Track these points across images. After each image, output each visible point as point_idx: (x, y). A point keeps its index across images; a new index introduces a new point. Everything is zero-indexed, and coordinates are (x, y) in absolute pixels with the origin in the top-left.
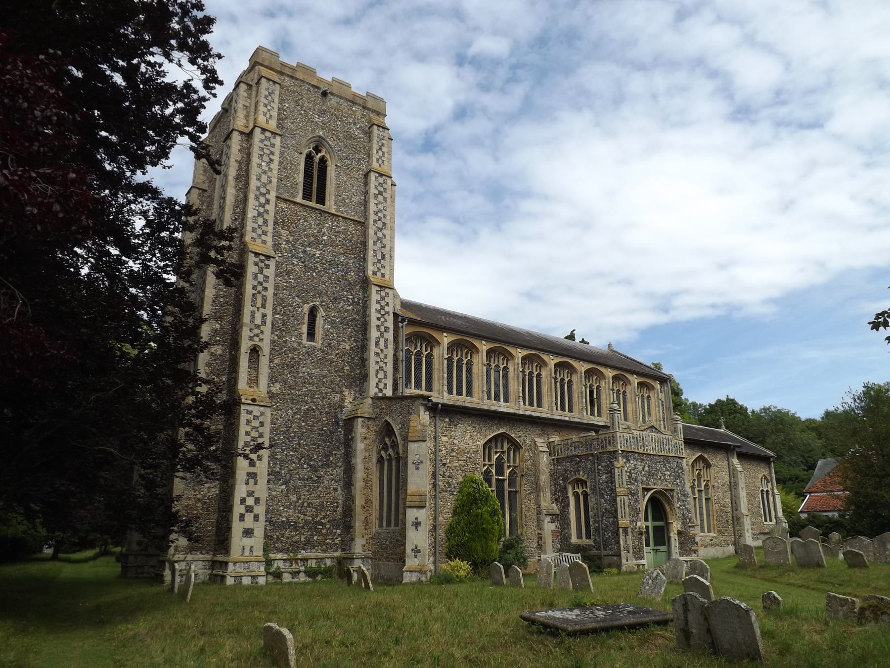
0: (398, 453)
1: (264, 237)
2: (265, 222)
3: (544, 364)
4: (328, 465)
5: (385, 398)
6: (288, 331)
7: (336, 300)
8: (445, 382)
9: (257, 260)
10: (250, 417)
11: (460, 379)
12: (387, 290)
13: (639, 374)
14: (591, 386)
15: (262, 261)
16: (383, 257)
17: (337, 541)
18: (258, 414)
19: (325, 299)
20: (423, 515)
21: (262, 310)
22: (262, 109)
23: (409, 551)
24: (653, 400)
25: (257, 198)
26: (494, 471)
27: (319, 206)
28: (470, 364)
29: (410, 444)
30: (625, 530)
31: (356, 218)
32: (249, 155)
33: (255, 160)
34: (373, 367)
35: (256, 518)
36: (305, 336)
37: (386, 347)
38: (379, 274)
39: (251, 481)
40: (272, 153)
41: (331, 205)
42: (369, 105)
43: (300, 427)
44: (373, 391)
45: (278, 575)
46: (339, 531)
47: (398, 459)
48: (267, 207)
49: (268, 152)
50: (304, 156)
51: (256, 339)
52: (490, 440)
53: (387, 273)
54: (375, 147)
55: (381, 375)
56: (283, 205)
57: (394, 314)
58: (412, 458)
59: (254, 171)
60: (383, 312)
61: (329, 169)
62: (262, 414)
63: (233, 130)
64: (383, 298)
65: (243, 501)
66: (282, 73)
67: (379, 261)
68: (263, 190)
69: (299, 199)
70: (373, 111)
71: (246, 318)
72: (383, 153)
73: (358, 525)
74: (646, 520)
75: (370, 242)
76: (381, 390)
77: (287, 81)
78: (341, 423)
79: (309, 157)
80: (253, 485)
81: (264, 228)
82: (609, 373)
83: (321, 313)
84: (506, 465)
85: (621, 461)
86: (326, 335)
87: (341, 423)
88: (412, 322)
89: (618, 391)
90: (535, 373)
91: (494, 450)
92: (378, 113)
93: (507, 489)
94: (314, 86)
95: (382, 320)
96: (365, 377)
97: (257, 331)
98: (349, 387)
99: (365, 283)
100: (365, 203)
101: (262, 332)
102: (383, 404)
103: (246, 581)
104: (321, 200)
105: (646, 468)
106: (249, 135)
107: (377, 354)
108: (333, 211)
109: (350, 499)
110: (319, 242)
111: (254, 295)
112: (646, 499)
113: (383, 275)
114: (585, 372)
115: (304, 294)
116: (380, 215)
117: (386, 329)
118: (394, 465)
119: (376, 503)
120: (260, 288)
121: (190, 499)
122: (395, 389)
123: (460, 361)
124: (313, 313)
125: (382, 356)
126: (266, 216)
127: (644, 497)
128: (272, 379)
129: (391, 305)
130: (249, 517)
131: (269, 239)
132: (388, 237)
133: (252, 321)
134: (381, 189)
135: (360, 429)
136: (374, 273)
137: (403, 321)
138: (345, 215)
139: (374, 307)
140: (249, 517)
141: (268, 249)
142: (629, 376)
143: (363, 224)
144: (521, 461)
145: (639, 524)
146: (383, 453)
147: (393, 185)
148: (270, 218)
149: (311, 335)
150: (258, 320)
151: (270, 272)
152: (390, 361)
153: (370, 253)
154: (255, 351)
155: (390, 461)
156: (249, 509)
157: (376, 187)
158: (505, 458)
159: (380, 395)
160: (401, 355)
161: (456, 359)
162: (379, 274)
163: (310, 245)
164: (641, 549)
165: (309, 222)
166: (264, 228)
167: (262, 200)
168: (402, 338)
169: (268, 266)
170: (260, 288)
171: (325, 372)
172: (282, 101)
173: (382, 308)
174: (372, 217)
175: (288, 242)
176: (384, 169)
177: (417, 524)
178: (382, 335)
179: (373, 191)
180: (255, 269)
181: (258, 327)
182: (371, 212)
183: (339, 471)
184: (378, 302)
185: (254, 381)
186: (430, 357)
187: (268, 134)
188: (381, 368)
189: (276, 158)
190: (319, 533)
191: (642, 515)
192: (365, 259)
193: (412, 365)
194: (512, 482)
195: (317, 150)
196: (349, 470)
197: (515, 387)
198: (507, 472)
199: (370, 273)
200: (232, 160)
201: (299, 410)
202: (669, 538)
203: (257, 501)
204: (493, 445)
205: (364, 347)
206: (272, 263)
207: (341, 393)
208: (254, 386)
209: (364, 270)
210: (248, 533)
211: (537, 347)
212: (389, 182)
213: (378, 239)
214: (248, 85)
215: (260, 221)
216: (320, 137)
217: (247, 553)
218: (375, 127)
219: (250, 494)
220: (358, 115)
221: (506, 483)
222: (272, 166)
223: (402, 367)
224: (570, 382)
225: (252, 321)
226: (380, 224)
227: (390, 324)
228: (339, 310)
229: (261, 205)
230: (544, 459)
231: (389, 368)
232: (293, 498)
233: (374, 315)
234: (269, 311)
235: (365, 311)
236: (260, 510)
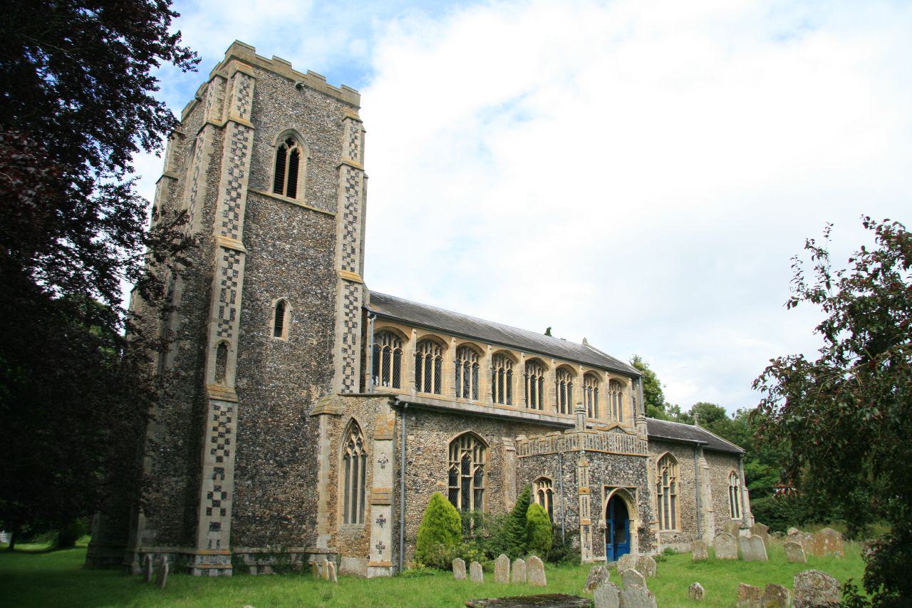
12: (356, 285)
27: (290, 200)
35: (223, 512)
51: (224, 334)
55: (348, 371)
83: (288, 308)
86: (294, 330)
104: (292, 193)
107: (345, 350)
116: (351, 208)
125: (350, 352)
128: (239, 375)
130: (216, 511)
136: (344, 268)
150: (227, 316)
156: (216, 504)
185: (220, 376)
188: (348, 364)
190: (285, 528)
198: (472, 471)
203: (224, 495)
207: (308, 389)
210: (215, 527)
215: (231, 215)
229: (233, 200)
232: (259, 493)
236: (227, 504)
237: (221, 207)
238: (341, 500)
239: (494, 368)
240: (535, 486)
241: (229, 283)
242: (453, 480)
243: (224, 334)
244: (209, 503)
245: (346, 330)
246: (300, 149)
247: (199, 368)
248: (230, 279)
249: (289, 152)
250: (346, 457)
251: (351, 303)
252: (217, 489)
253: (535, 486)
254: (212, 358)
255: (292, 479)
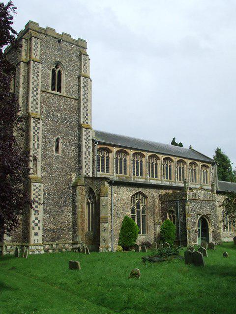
0: (96, 201)
1: (36, 110)
2: (37, 103)
3: (158, 158)
5: (89, 178)
6: (47, 150)
7: (67, 135)
9: (34, 121)
10: (35, 188)
11: (121, 166)
12: (89, 130)
13: (202, 161)
14: (180, 168)
15: (36, 121)
16: (87, 115)
17: (70, 237)
18: (38, 186)
19: (63, 135)
21: (37, 142)
23: (101, 240)
24: (208, 172)
25: (33, 93)
27: (58, 93)
28: (125, 160)
29: (102, 198)
31: (75, 97)
33: (31, 76)
34: (84, 164)
35: (39, 228)
36: (54, 151)
37: (89, 155)
38: (85, 123)
39: (37, 214)
40: (38, 72)
41: (64, 92)
42: (79, 44)
43: (54, 190)
46: (71, 233)
47: (96, 203)
48: (37, 96)
49: (36, 71)
50: (51, 70)
52: (134, 195)
53: (89, 122)
55: (87, 167)
56: (44, 94)
57: (92, 139)
58: (102, 203)
59: (31, 80)
60: (87, 140)
61: (62, 75)
62: (40, 186)
63: (20, 62)
64: (87, 133)
65: (34, 222)
66: (41, 33)
67: (85, 117)
68: (35, 89)
69: (50, 91)
70: (81, 47)
72: (86, 67)
74: (198, 226)
76: (87, 174)
77: (43, 36)
78: (71, 188)
79: (54, 71)
80: (38, 217)
81: (36, 106)
82: (188, 162)
83: (61, 141)
84: (141, 204)
86: (63, 150)
88: (100, 143)
89: (192, 169)
90: (155, 163)
91: (135, 199)
92: (83, 48)
93: (141, 214)
94: (55, 38)
95: (87, 143)
97: (35, 151)
98: (74, 172)
99: (80, 127)
100: (79, 90)
101: (38, 151)
103: (36, 253)
104: (59, 90)
105: (199, 206)
106: (28, 63)
108: (65, 95)
110: (59, 110)
111: (34, 136)
112: (199, 218)
113: (87, 123)
114: (177, 161)
115: (53, 132)
117: (89, 147)
118: (96, 206)
119: (87, 221)
120: (36, 133)
121: (165, 268)
122: (93, 173)
123: (121, 159)
124: (57, 141)
125: (88, 159)
126: (37, 100)
127: (198, 217)
128: (42, 171)
129: (91, 136)
130: (36, 228)
131: (39, 110)
132: (89, 106)
133: (34, 147)
134: (85, 84)
136: (84, 122)
137: (96, 143)
138: (70, 96)
139: (84, 137)
140: (36, 228)
142: (197, 163)
143: (79, 100)
145: (195, 228)
146: (89, 200)
147: (91, 81)
148: (39, 101)
149: (57, 150)
150: (36, 147)
151: (40, 126)
152: (91, 161)
153: (82, 113)
154: (35, 159)
156: (36, 225)
157: (83, 83)
159: (87, 176)
160: (96, 158)
161: (119, 158)
162: (85, 123)
163: (55, 111)
164: (196, 239)
165: (54, 101)
166: (36, 106)
167: (35, 93)
168: (96, 150)
169: (39, 123)
170: (36, 133)
171: (63, 167)
172: (41, 46)
173: (87, 138)
174: (82, 97)
175: (46, 110)
176: (87, 74)
178: (87, 150)
179: (82, 85)
180: (34, 125)
181: (36, 149)
182: (82, 95)
183: (70, 208)
184: (85, 135)
186: (108, 158)
187: (36, 63)
188: (87, 164)
189: (40, 74)
190: (63, 234)
191: (196, 225)
192: (79, 116)
193: (101, 163)
194: (143, 212)
195: (57, 67)
197: (145, 169)
198: (141, 208)
199: (82, 122)
200: (21, 75)
202: (208, 234)
203: (39, 221)
204: (135, 196)
205: (80, 155)
206: (41, 121)
207: (70, 175)
209: (79, 121)
210: (36, 234)
211: (155, 151)
212: (89, 80)
213: (85, 107)
214: (26, 39)
215: (35, 103)
216: (58, 61)
217: (36, 242)
218: (82, 55)
219: (36, 219)
220: (75, 49)
221: (141, 212)
222: (38, 78)
223: (96, 163)
224: (170, 166)
225: (34, 147)
226: (85, 100)
227: (91, 145)
228: (68, 139)
231: (91, 164)
232: (52, 219)
233: (84, 141)
234: (40, 143)
236: (40, 225)
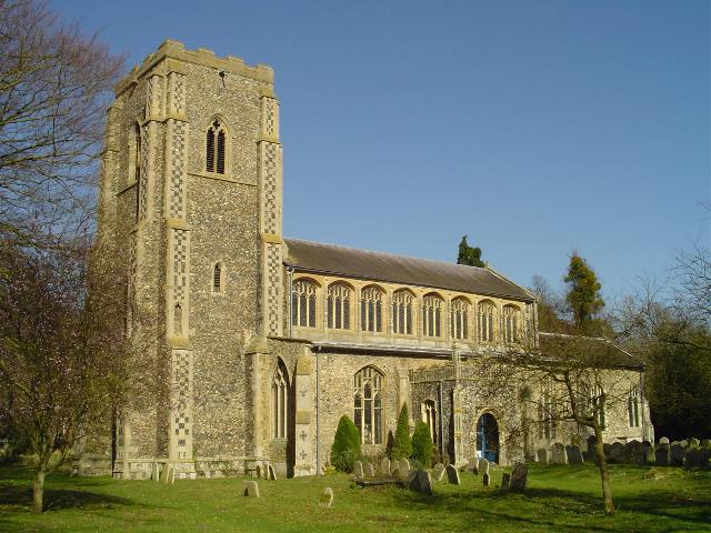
4: (233, 390)
8: (326, 319)
12: (277, 246)
20: (306, 429)
22: (173, 101)
25: (173, 180)
26: (363, 395)
27: (219, 176)
30: (459, 440)
32: (164, 141)
33: (170, 147)
34: (266, 311)
35: (187, 431)
36: (212, 289)
44: (267, 331)
45: (203, 474)
51: (179, 298)
54: (266, 117)
55: (273, 318)
59: (170, 157)
68: (178, 173)
69: (204, 173)
71: (171, 282)
73: (259, 435)
75: (263, 205)
76: (273, 330)
79: (211, 133)
83: (223, 269)
84: (373, 389)
85: (459, 386)
86: (229, 287)
87: (243, 357)
96: (260, 320)
100: (258, 168)
102: (277, 343)
104: (221, 170)
107: (270, 301)
109: (251, 415)
113: (273, 232)
116: (271, 179)
118: (287, 378)
125: (274, 301)
128: (191, 326)
130: (182, 431)
135: (258, 362)
136: (266, 231)
139: (267, 261)
141: (183, 223)
144: (385, 385)
149: (217, 285)
150: (180, 283)
153: (263, 213)
155: (282, 387)
156: (182, 426)
158: (372, 384)
160: (290, 299)
165: (212, 192)
167: (177, 181)
177: (304, 436)
179: (264, 158)
181: (180, 288)
183: (241, 395)
185: (179, 329)
188: (273, 312)
190: (229, 442)
194: (377, 402)
196: (250, 395)
198: (374, 395)
199: (263, 231)
201: (210, 348)
203: (187, 419)
205: (259, 295)
207: (242, 333)
208: (179, 331)
210: (182, 442)
215: (177, 199)
217: (182, 457)
226: (270, 188)
228: (237, 264)
229: (177, 186)
230: (405, 383)
231: (280, 311)
232: (209, 416)
235: (259, 264)
236: (189, 426)
237: (169, 194)
238: (151, 202)
239: (395, 305)
240: (423, 406)
241: (179, 257)
242: (358, 403)
243: (179, 298)
244: (177, 426)
245: (270, 284)
246: (226, 131)
247: (160, 323)
248: (180, 253)
249: (216, 134)
250: (275, 386)
251: (274, 262)
252: (182, 415)
253: (423, 406)
254: (171, 316)
255: (233, 404)
